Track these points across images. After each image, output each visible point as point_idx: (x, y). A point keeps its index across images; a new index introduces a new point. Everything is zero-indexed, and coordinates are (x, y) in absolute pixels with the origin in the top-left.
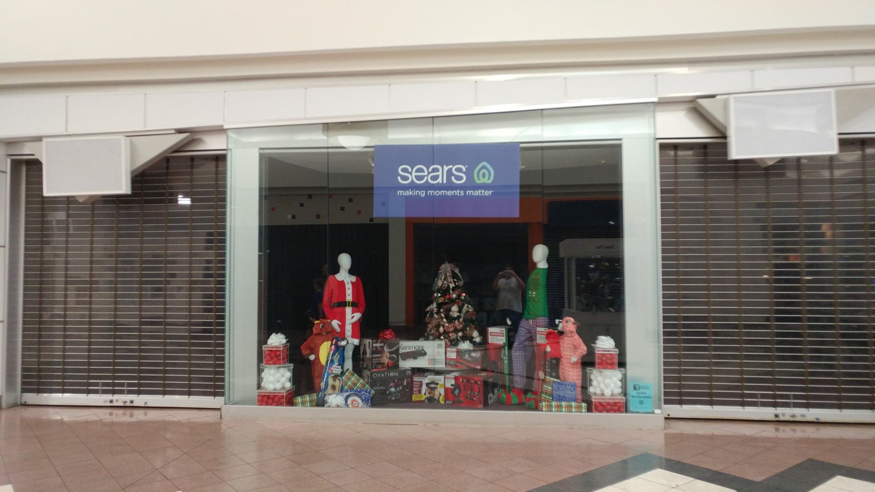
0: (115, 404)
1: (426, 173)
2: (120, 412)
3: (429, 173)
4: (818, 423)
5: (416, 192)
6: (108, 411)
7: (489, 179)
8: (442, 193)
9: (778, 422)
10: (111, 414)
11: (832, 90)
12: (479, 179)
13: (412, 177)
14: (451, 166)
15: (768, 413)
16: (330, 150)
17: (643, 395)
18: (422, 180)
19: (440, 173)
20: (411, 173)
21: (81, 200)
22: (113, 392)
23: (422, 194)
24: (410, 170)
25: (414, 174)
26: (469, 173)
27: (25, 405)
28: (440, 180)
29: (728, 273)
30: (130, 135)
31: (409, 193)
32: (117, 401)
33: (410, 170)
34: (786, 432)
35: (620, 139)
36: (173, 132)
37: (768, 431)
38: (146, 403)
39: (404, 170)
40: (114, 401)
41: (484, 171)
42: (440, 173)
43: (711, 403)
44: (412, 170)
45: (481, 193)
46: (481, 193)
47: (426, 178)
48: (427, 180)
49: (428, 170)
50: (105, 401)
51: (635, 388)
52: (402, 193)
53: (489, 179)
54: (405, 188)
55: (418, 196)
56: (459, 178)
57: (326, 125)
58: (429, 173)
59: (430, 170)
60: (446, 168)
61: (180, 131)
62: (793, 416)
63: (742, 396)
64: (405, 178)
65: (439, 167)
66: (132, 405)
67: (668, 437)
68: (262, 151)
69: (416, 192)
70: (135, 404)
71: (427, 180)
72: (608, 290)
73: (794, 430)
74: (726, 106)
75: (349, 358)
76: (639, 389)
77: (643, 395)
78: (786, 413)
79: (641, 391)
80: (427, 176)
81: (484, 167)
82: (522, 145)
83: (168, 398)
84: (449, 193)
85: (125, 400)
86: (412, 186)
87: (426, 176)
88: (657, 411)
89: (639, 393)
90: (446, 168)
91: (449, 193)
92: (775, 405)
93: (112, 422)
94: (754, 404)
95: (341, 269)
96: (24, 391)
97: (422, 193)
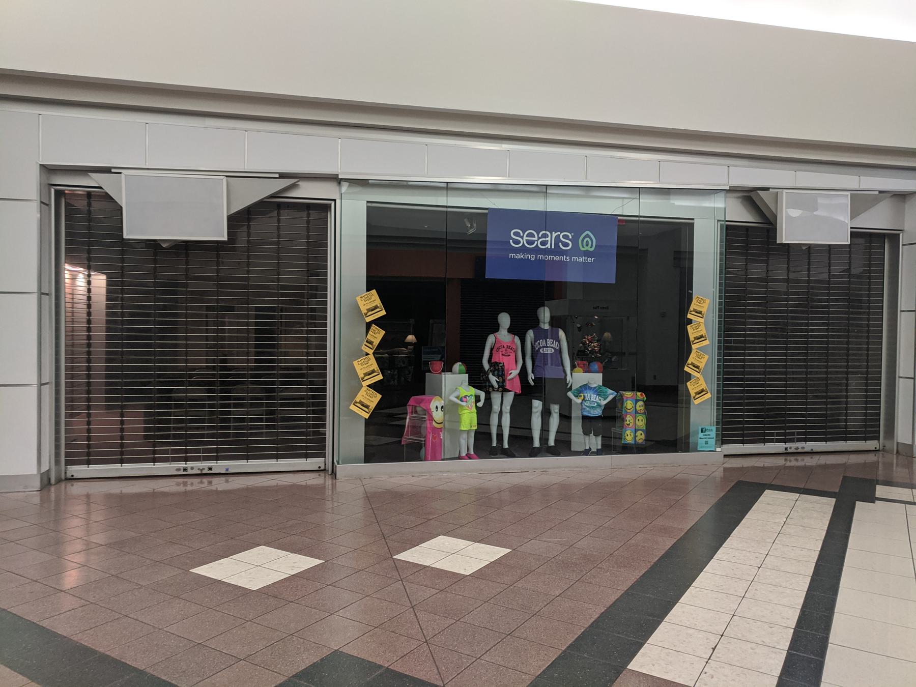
0: (190, 472)
1: (536, 238)
2: (196, 481)
3: (539, 238)
4: (812, 453)
5: (527, 256)
6: (180, 480)
7: (591, 247)
8: (551, 257)
9: (786, 454)
10: (185, 484)
11: (848, 193)
12: (583, 247)
13: (523, 241)
14: (559, 233)
15: (780, 447)
16: (449, 209)
17: (709, 437)
18: (563, 246)
19: (549, 239)
20: (522, 237)
21: (164, 246)
22: (186, 460)
23: (532, 258)
24: (522, 235)
25: (525, 238)
26: (575, 240)
27: (73, 479)
28: (548, 246)
29: (816, 337)
30: (231, 176)
31: (520, 256)
32: (192, 468)
33: (522, 235)
34: (792, 462)
35: (693, 219)
36: (277, 176)
37: (780, 461)
38: (227, 470)
39: (516, 234)
40: (189, 469)
41: (587, 239)
42: (549, 239)
43: (743, 442)
44: (524, 234)
45: (585, 259)
46: (585, 259)
47: (536, 242)
48: (537, 244)
49: (538, 235)
50: (178, 470)
51: (702, 431)
52: (576, 259)
53: (591, 247)
54: (517, 251)
55: (529, 260)
56: (566, 245)
57: (446, 183)
58: (539, 238)
59: (540, 236)
60: (554, 235)
61: (283, 176)
62: (797, 448)
63: (764, 435)
64: (517, 242)
65: (547, 233)
66: (210, 472)
67: (725, 470)
68: (370, 205)
69: (527, 256)
70: (214, 471)
71: (537, 244)
72: (597, 349)
73: (797, 460)
74: (776, 197)
75: (506, 413)
76: (705, 431)
77: (709, 437)
78: (792, 446)
79: (707, 433)
80: (537, 241)
81: (587, 236)
82: (619, 218)
83: (252, 462)
84: (557, 258)
85: (201, 468)
86: (523, 249)
87: (536, 241)
88: (718, 449)
89: (705, 435)
90: (554, 235)
91: (557, 258)
92: (785, 441)
93: (743, 467)
94: (771, 441)
95: (500, 328)
96: (68, 463)
97: (533, 257)
